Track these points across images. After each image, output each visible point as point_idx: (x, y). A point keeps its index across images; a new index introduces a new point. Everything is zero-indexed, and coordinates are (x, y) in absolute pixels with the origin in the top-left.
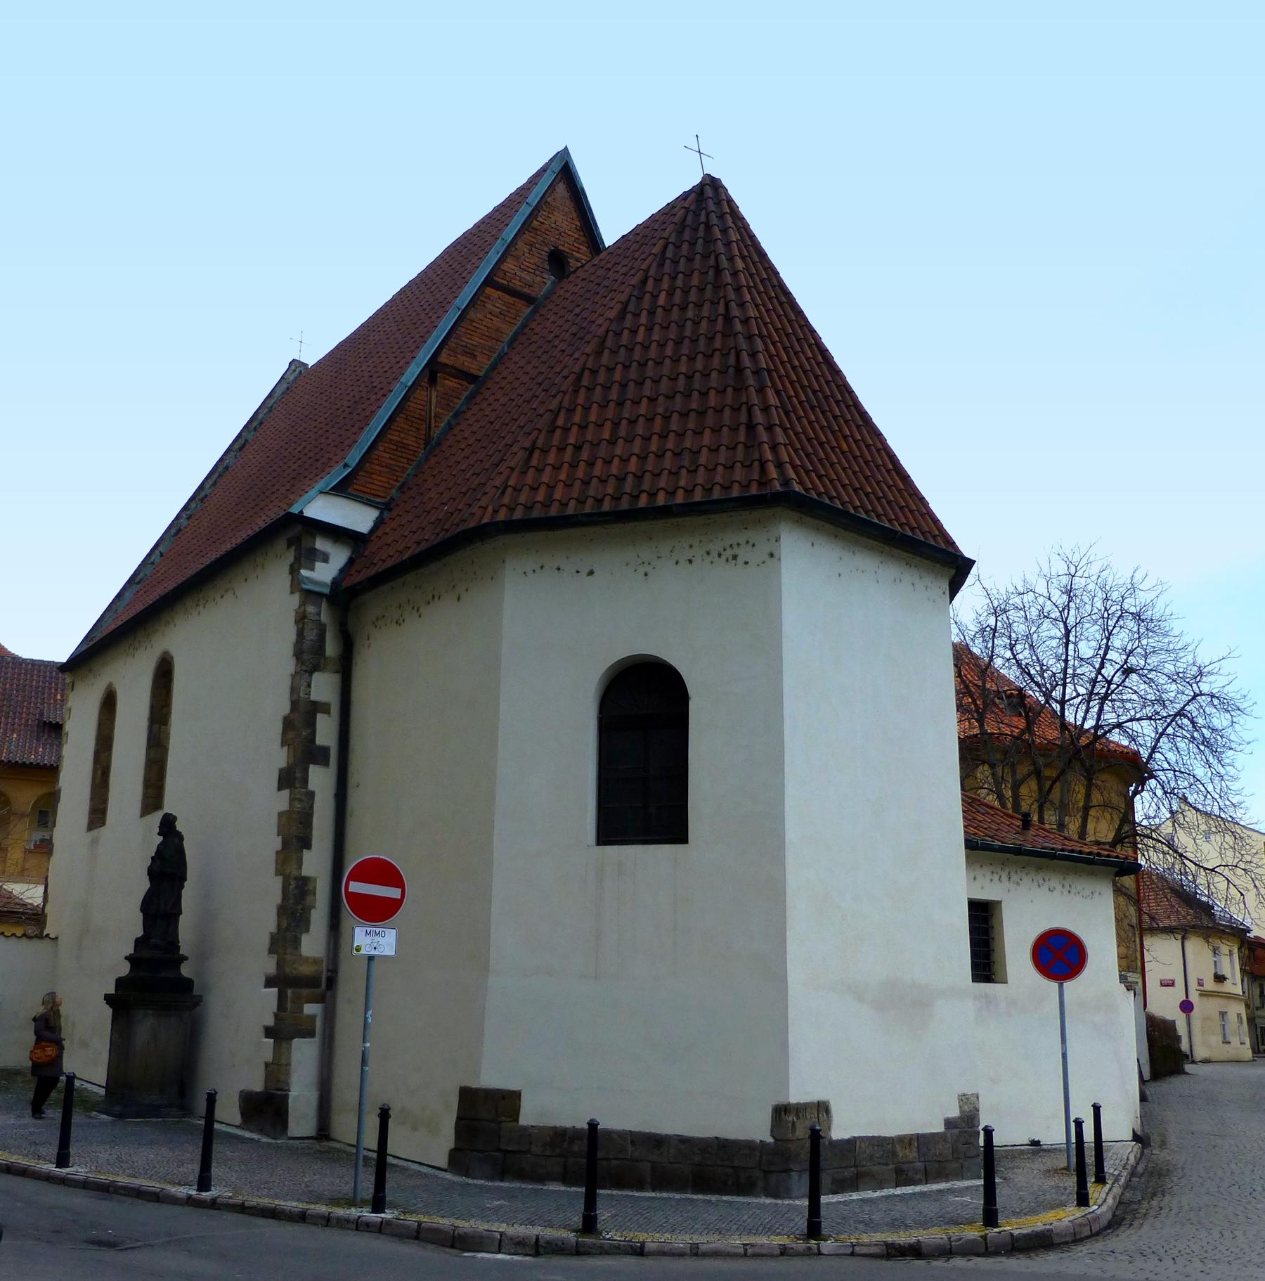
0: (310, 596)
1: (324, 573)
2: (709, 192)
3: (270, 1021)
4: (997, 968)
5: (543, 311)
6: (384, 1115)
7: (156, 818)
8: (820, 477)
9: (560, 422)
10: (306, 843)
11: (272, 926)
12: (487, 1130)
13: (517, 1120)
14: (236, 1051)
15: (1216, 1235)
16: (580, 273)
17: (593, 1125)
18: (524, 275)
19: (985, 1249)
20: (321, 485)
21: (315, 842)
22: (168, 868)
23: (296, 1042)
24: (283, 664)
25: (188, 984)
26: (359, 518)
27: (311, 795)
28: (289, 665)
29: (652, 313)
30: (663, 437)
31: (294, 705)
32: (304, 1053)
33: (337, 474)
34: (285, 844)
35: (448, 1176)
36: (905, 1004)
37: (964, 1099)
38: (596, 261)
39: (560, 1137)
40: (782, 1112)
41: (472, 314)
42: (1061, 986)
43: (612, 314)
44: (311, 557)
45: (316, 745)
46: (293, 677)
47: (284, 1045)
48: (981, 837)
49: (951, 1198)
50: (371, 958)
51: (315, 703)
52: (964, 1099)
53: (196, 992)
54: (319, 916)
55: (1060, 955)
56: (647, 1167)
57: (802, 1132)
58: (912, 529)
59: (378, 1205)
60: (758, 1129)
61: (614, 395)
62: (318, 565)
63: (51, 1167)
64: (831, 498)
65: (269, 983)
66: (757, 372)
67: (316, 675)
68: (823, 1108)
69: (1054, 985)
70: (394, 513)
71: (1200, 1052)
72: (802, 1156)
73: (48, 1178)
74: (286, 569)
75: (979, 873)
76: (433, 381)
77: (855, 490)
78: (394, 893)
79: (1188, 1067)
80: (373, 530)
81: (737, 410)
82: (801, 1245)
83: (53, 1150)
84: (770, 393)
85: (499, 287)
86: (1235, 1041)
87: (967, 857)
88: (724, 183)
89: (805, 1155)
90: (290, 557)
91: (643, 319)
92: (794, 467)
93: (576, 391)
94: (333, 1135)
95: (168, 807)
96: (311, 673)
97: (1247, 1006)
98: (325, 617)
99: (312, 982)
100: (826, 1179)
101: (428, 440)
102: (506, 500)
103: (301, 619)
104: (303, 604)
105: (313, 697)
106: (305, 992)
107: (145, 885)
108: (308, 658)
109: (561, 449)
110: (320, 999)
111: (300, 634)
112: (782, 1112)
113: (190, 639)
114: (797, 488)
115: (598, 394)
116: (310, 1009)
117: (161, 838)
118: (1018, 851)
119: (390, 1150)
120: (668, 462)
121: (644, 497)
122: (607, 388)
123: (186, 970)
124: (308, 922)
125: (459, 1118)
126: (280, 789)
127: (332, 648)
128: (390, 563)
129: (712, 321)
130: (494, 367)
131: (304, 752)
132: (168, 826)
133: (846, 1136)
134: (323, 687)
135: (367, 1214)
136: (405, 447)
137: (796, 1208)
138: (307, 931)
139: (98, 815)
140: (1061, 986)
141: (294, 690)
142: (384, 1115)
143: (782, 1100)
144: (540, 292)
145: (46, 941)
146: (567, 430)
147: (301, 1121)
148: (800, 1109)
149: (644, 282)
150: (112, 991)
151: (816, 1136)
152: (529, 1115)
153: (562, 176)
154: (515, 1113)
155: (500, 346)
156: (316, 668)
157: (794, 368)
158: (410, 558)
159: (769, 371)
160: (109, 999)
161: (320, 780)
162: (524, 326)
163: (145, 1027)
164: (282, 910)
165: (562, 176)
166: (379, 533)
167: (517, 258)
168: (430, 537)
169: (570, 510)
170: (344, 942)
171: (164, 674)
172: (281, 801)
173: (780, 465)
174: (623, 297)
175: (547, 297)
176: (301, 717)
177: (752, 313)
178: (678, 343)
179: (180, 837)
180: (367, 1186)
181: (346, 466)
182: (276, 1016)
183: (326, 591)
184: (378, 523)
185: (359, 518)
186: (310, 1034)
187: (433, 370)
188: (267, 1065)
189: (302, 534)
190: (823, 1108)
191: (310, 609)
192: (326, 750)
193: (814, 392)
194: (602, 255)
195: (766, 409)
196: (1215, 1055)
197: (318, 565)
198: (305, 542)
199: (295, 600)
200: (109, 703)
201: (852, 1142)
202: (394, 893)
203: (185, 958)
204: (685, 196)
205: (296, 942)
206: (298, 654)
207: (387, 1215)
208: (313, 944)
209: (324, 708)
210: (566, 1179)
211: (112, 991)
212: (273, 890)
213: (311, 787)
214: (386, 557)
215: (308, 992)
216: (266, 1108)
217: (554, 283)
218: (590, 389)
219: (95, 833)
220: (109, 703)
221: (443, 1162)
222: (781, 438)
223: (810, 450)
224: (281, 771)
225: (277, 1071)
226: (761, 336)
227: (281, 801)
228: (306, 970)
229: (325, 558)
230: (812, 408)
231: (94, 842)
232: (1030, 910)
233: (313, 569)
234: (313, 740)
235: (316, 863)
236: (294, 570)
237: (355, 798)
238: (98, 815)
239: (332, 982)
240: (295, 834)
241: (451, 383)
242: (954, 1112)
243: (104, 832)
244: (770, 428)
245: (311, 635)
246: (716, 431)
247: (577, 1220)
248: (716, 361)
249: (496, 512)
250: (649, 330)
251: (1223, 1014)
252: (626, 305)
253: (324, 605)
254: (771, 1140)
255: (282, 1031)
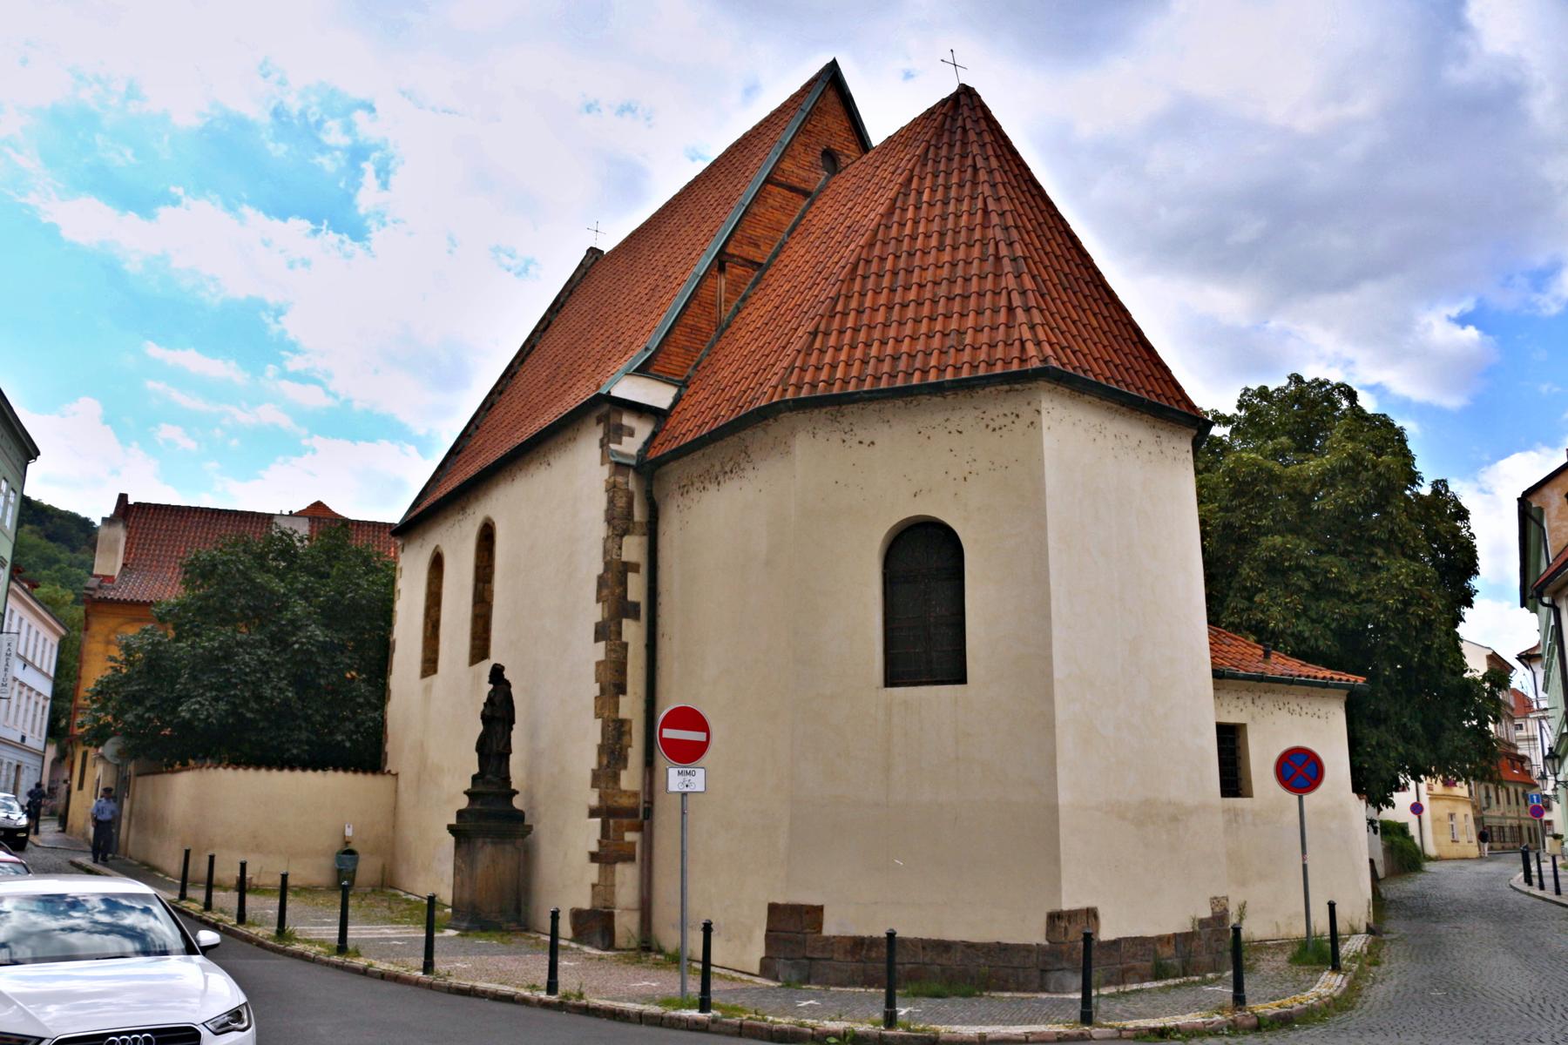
0: (619, 467)
1: (630, 446)
2: (963, 99)
3: (595, 848)
4: (1243, 783)
5: (818, 204)
6: (707, 929)
7: (485, 667)
8: (1074, 352)
9: (839, 308)
10: (621, 689)
11: (594, 764)
12: (794, 935)
13: (820, 931)
14: (568, 868)
15: (1437, 1013)
16: (850, 169)
17: (891, 935)
18: (800, 172)
19: (1234, 1028)
20: (624, 366)
21: (629, 689)
22: (499, 712)
23: (619, 867)
24: (596, 529)
25: (519, 816)
26: (659, 395)
27: (626, 645)
28: (600, 529)
29: (917, 208)
30: (932, 319)
31: (607, 565)
32: (627, 877)
33: (638, 357)
34: (602, 690)
35: (758, 980)
36: (1156, 818)
37: (1215, 901)
38: (864, 159)
39: (859, 945)
40: (1054, 918)
41: (755, 209)
42: (1300, 799)
43: (881, 210)
44: (615, 432)
45: (631, 602)
46: (606, 540)
47: (599, 903)
48: (1227, 666)
49: (1205, 988)
50: (684, 794)
51: (625, 564)
52: (1215, 901)
53: (527, 822)
54: (635, 754)
55: (1300, 770)
56: (937, 969)
57: (1075, 934)
58: (1158, 396)
59: (1534, 739)
60: (1034, 933)
61: (886, 282)
62: (625, 439)
63: (420, 974)
64: (1085, 372)
65: (593, 813)
66: (1014, 260)
67: (626, 539)
68: (1091, 914)
69: (1295, 798)
70: (690, 391)
71: (1431, 850)
72: (1076, 953)
73: (417, 983)
74: (597, 443)
75: (1227, 699)
76: (722, 269)
77: (1106, 363)
78: (699, 736)
79: (1428, 866)
80: (672, 407)
81: (996, 294)
82: (1075, 1031)
83: (420, 962)
84: (1027, 279)
85: (779, 184)
86: (1463, 839)
87: (1216, 689)
88: (978, 90)
89: (1078, 955)
90: (598, 433)
91: (910, 214)
92: (1051, 345)
93: (853, 280)
94: (655, 947)
95: (496, 657)
96: (622, 537)
97: (1474, 807)
98: (632, 485)
99: (631, 812)
100: (1096, 976)
101: (718, 325)
102: (793, 380)
103: (612, 488)
104: (613, 474)
105: (624, 558)
106: (625, 821)
107: (479, 728)
108: (619, 523)
109: (841, 332)
110: (639, 828)
111: (611, 501)
112: (1054, 918)
113: (504, 507)
114: (1054, 363)
115: (871, 283)
116: (630, 837)
117: (491, 686)
118: (1261, 678)
119: (713, 961)
120: (936, 342)
121: (917, 375)
122: (880, 276)
123: (517, 802)
124: (626, 759)
125: (769, 930)
126: (597, 640)
127: (639, 514)
128: (689, 438)
129: (971, 214)
130: (775, 255)
131: (620, 609)
132: (497, 674)
133: (1113, 938)
134: (633, 550)
135: (694, 1013)
136: (699, 330)
137: (1071, 1001)
138: (625, 767)
139: (430, 665)
140: (1300, 799)
141: (606, 552)
142: (707, 929)
143: (1049, 909)
144: (814, 187)
145: (389, 777)
146: (845, 314)
147: (626, 923)
148: (1072, 915)
149: (910, 180)
150: (453, 821)
151: (1088, 938)
152: (830, 928)
153: (830, 84)
154: (819, 925)
155: (781, 236)
156: (626, 532)
157: (1047, 254)
158: (710, 433)
159: (1025, 258)
160: (451, 829)
161: (633, 632)
162: (802, 217)
163: (486, 853)
164: (602, 749)
165: (830, 84)
166: (679, 408)
167: (794, 158)
168: (726, 414)
169: (851, 388)
170: (658, 785)
171: (487, 536)
172: (599, 651)
173: (1038, 344)
174: (891, 194)
175: (821, 191)
176: (614, 576)
177: (1007, 206)
178: (942, 235)
179: (508, 684)
180: (694, 987)
181: (647, 349)
182: (600, 842)
183: (633, 462)
184: (677, 399)
185: (659, 395)
186: (631, 859)
187: (721, 262)
188: (594, 886)
189: (607, 411)
190: (1091, 914)
191: (620, 479)
192: (637, 605)
193: (1066, 275)
194: (871, 154)
195: (1023, 293)
196: (1446, 853)
197: (625, 439)
198: (614, 419)
199: (605, 472)
200: (437, 563)
201: (1116, 943)
202: (699, 736)
203: (516, 792)
204: (944, 102)
205: (616, 778)
206: (610, 519)
207: (714, 1013)
208: (630, 779)
209: (634, 567)
210: (869, 982)
211: (453, 821)
212: (592, 732)
213: (624, 639)
214: (686, 429)
215: (627, 823)
216: (595, 925)
217: (827, 178)
218: (865, 278)
219: (428, 680)
220: (437, 563)
221: (756, 969)
222: (1038, 319)
223: (1064, 328)
224: (597, 625)
225: (603, 889)
226: (1017, 227)
227: (599, 651)
228: (625, 802)
229: (631, 434)
230: (1065, 289)
231: (428, 690)
232: (1273, 731)
233: (620, 443)
234: (625, 597)
235: (631, 707)
236: (603, 445)
237: (666, 649)
238: (430, 665)
239: (649, 812)
240: (613, 683)
241: (738, 271)
242: (1206, 913)
243: (436, 680)
244: (1028, 310)
245: (621, 502)
246: (979, 313)
247: (879, 1016)
248: (976, 252)
249: (785, 390)
250: (916, 223)
251: (1452, 816)
252: (894, 200)
253: (631, 475)
254: (1046, 943)
255: (605, 857)
